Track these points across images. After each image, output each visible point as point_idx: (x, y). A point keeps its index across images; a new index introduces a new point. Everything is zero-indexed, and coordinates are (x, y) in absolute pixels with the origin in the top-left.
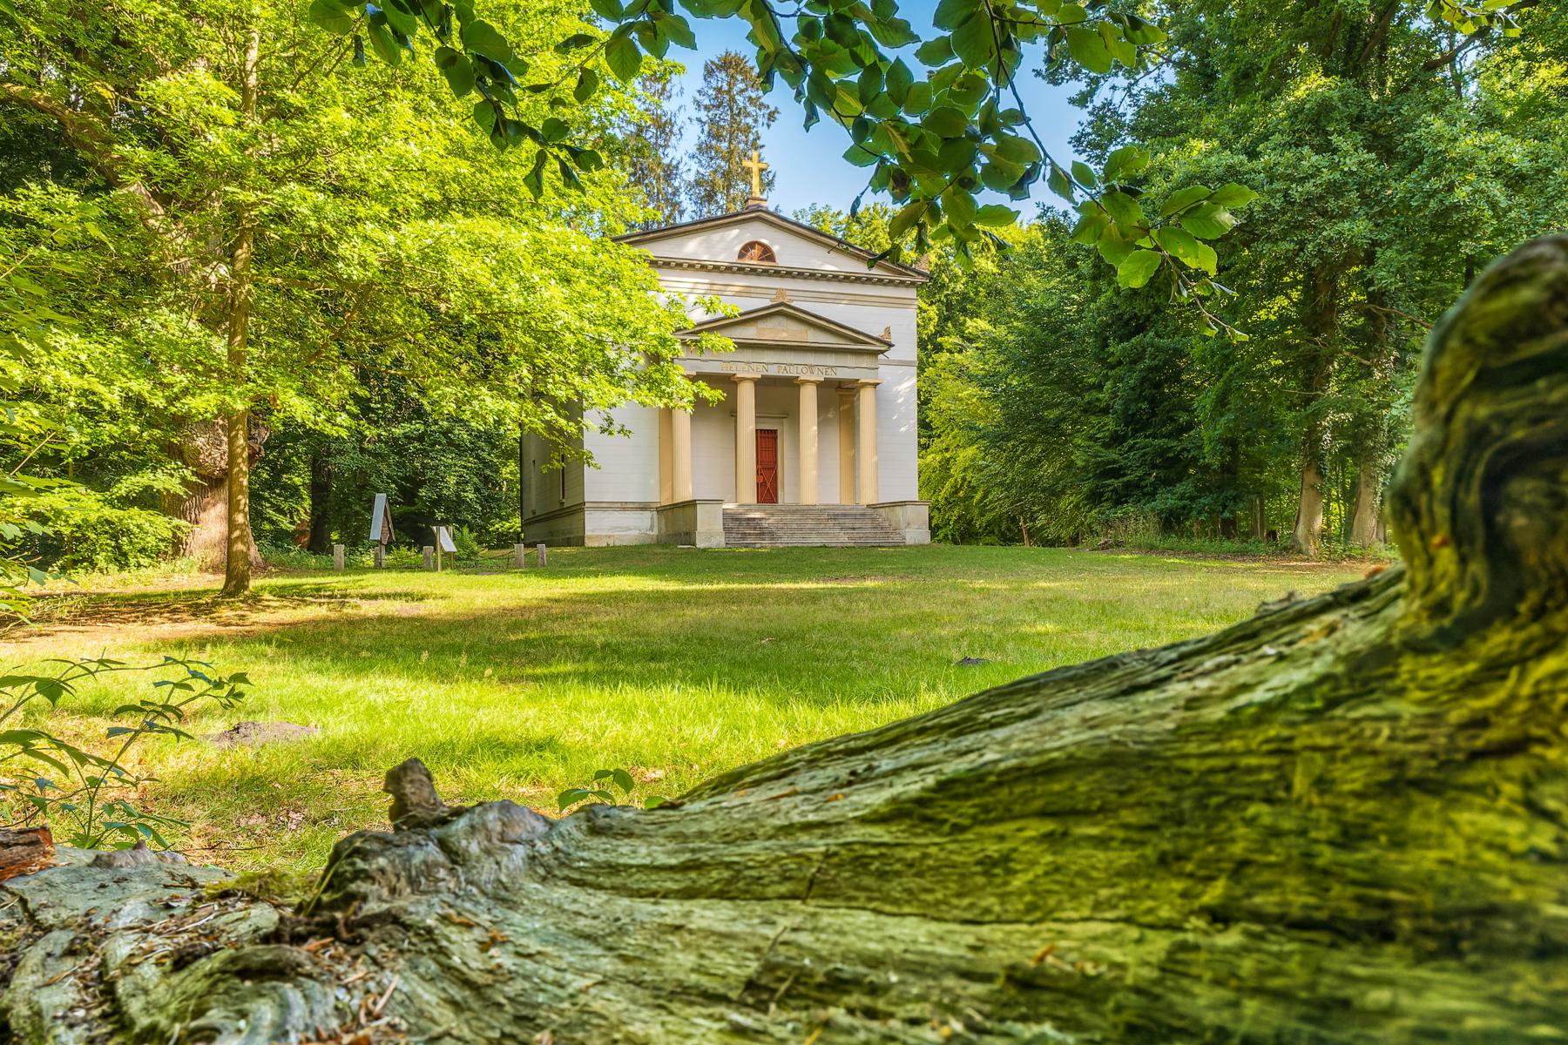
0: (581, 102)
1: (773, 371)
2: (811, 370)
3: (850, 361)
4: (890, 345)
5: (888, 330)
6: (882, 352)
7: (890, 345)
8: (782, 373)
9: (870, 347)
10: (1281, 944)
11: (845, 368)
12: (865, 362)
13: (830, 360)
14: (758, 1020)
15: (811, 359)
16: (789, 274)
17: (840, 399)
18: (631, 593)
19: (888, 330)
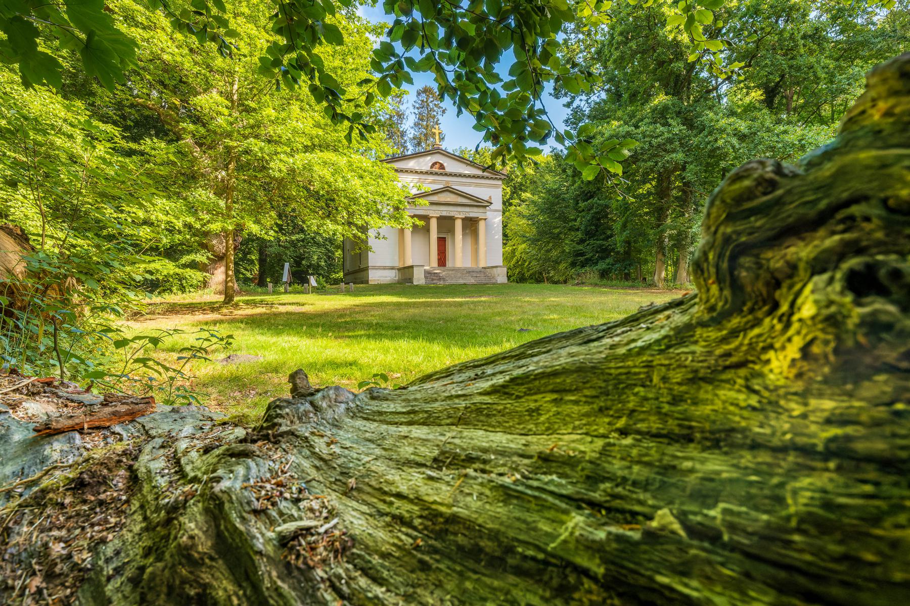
1: (444, 214)
2: (459, 213)
3: (475, 209)
9: (483, 204)
11: (473, 213)
12: (481, 210)
13: (467, 209)
15: (459, 209)
16: (451, 175)
17: (471, 225)
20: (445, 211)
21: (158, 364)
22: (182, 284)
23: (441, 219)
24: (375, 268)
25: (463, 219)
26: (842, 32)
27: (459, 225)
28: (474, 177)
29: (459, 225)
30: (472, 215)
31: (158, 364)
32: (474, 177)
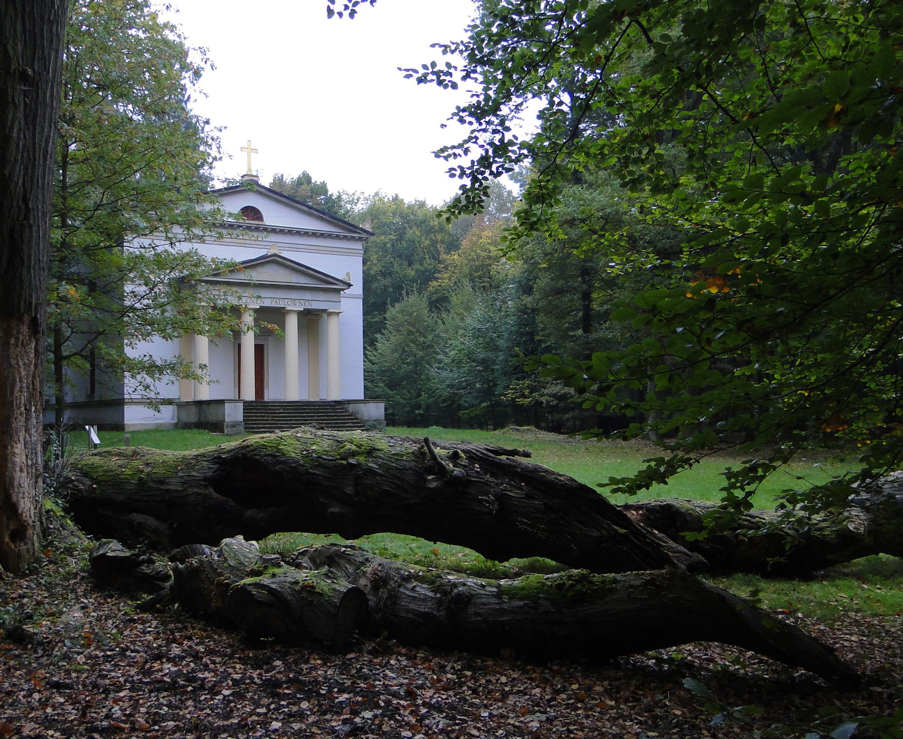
0: (583, 267)
1: (268, 303)
2: (294, 303)
3: (322, 296)
4: (350, 285)
5: (348, 274)
6: (343, 290)
7: (350, 285)
8: (274, 305)
9: (332, 286)
10: (570, 577)
11: (317, 302)
12: (331, 297)
13: (308, 296)
14: (328, 560)
15: (294, 295)
16: (274, 231)
17: (311, 321)
18: (472, 427)
19: (348, 274)
20: (270, 300)
21: (248, 228)
22: (436, 555)
23: (262, 313)
24: (133, 402)
25: (300, 313)
26: (688, 98)
27: (292, 323)
28: (315, 234)
29: (292, 323)
30: (315, 306)
31: (248, 228)
32: (315, 234)
